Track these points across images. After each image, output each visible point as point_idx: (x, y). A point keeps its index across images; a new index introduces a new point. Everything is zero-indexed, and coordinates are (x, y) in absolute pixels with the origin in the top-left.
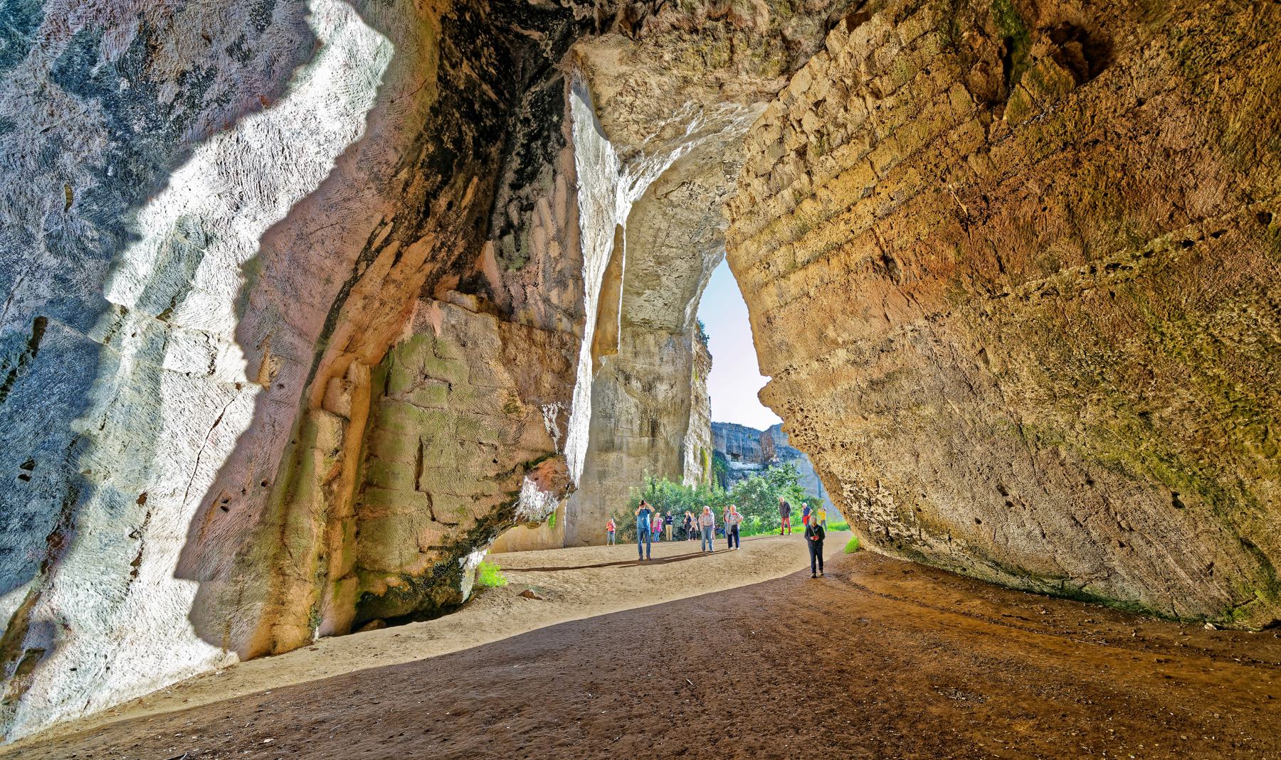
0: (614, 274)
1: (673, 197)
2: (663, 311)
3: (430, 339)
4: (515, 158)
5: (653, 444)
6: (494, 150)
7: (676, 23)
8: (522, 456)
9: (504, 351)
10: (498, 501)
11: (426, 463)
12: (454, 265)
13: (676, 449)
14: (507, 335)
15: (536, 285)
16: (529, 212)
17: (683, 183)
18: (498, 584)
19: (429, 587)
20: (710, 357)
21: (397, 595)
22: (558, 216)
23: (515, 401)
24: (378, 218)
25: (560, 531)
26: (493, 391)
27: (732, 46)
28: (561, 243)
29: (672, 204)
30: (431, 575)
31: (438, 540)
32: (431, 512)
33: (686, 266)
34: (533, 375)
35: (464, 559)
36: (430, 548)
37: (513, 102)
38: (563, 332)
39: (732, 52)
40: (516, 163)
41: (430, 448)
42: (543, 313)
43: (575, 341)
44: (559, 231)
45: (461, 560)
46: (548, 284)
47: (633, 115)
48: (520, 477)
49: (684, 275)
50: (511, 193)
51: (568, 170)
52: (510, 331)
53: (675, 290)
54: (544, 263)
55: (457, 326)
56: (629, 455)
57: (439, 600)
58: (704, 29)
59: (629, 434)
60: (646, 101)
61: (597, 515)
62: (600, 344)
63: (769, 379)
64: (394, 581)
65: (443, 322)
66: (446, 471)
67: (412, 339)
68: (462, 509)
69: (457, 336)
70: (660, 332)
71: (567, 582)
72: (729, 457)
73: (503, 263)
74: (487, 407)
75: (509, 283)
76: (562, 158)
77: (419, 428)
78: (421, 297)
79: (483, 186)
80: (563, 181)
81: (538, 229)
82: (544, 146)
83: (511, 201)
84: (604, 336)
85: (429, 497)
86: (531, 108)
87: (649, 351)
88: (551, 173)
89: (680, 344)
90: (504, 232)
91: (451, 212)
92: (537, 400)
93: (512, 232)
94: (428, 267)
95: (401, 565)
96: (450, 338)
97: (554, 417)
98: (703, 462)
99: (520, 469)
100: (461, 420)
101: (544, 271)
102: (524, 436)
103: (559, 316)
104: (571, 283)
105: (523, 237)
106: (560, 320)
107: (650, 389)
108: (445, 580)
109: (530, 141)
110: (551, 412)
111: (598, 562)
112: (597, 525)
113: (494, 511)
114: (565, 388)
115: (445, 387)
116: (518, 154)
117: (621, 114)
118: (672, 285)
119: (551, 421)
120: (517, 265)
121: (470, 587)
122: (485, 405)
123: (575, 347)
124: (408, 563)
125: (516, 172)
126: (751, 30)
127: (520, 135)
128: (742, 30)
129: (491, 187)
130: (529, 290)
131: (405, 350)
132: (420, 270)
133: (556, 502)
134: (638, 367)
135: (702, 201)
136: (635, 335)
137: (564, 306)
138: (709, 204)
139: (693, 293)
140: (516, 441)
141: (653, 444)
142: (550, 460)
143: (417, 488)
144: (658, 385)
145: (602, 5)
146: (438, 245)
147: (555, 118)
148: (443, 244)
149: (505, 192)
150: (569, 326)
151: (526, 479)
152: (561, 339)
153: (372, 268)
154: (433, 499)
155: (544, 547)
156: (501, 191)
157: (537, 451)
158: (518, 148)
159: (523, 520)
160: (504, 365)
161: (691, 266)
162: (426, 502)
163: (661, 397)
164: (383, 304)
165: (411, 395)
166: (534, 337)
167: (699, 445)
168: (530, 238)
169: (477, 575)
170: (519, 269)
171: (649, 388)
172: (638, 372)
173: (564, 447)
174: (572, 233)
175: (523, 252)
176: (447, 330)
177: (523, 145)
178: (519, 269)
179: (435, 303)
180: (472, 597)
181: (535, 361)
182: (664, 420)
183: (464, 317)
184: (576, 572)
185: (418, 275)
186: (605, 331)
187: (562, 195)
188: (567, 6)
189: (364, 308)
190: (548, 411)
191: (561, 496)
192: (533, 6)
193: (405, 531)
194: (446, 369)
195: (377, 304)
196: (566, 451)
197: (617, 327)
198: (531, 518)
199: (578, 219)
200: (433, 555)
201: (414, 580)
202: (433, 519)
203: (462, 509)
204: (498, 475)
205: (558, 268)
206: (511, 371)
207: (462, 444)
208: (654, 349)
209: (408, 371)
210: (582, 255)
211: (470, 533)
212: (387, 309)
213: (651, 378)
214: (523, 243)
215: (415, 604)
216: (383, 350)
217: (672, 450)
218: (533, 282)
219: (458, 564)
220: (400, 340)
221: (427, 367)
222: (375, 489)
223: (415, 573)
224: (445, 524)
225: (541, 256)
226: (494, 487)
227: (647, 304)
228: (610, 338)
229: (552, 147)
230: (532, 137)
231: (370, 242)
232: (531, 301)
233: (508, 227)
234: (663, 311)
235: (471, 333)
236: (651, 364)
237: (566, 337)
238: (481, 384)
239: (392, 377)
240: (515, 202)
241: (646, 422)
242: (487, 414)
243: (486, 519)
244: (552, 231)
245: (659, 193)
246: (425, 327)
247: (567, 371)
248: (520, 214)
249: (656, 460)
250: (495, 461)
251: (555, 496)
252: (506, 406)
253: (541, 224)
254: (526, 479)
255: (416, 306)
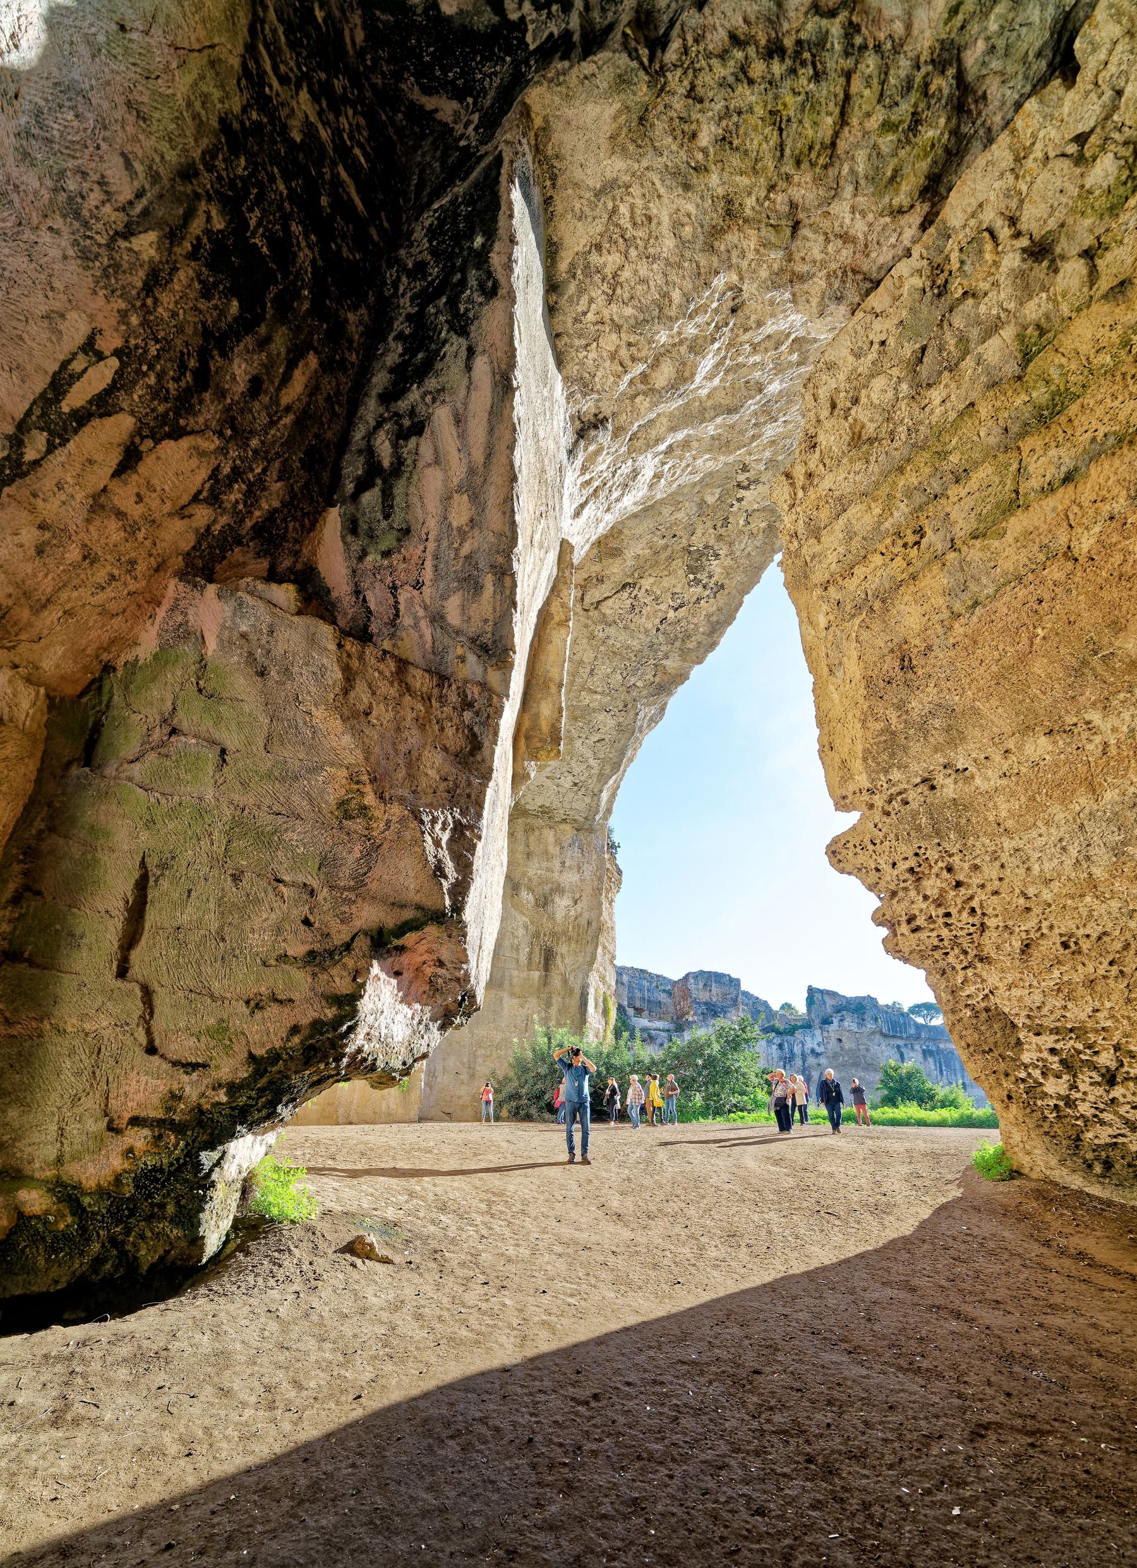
0: (557, 619)
1: (607, 608)
2: (571, 795)
3: (193, 657)
4: (392, 345)
5: (545, 981)
6: (355, 320)
7: (742, 29)
8: (368, 915)
9: (346, 692)
10: (306, 1015)
11: (152, 917)
12: (258, 530)
13: (577, 991)
14: (355, 664)
15: (418, 585)
16: (413, 441)
17: (624, 586)
18: (294, 1214)
19: (118, 1222)
20: (620, 872)
21: (37, 1238)
22: (471, 440)
23: (363, 794)
24: (76, 330)
25: (414, 1096)
26: (316, 769)
27: (847, 97)
28: (476, 499)
29: (605, 622)
30: (128, 1190)
31: (155, 1100)
32: (149, 1032)
33: (611, 723)
34: (403, 748)
35: (215, 1155)
36: (135, 1121)
37: (399, 237)
38: (466, 682)
39: (843, 119)
40: (394, 353)
41: (165, 884)
42: (429, 645)
43: (490, 699)
44: (472, 471)
45: (207, 1158)
46: (442, 585)
47: (614, 307)
48: (362, 963)
49: (607, 737)
50: (381, 410)
51: (499, 344)
52: (361, 658)
53: (592, 762)
54: (438, 540)
55: (252, 637)
56: (512, 994)
57: (147, 1255)
58: (799, 42)
59: (513, 965)
60: (643, 271)
61: (464, 1077)
62: (527, 738)
63: (854, 817)
64: (34, 1200)
65: (223, 627)
66: (195, 937)
67: (156, 657)
68: (220, 1031)
69: (250, 654)
70: (563, 826)
71: (443, 1208)
72: (630, 1011)
73: (356, 546)
74: (300, 803)
75: (364, 585)
76: (490, 317)
77: (144, 836)
78: (182, 575)
79: (327, 385)
80: (487, 368)
81: (429, 471)
82: (453, 303)
83: (379, 425)
84: (535, 725)
85: (147, 994)
86: (430, 242)
87: (546, 852)
88: (464, 354)
89: (589, 844)
90: (363, 485)
91: (257, 406)
92: (410, 797)
93: (379, 482)
94: (203, 515)
95: (59, 1161)
96: (235, 659)
97: (445, 837)
98: (605, 1012)
99: (362, 944)
100: (239, 826)
101: (436, 557)
102: (378, 871)
103: (460, 651)
104: (488, 581)
105: (399, 489)
106: (463, 659)
107: (545, 904)
108: (162, 1206)
109: (423, 307)
110: (438, 826)
111: (494, 1161)
112: (463, 1091)
113: (296, 1040)
114: (469, 784)
115: (212, 755)
116: (400, 337)
117: (591, 301)
118: (589, 754)
119: (437, 843)
120: (383, 547)
121: (226, 1224)
122: (296, 799)
123: (491, 710)
124: (76, 1157)
125: (391, 371)
126: (896, 50)
127: (405, 302)
128: (878, 48)
129: (344, 399)
130: (404, 596)
131: (139, 677)
132: (182, 512)
133: (436, 1034)
134: (531, 873)
135: (648, 618)
136: (528, 830)
137: (472, 630)
138: (658, 621)
139: (616, 766)
140: (359, 882)
141: (545, 981)
142: (431, 930)
143: (122, 972)
144: (557, 899)
145: (587, 7)
146: (226, 470)
147: (479, 241)
148: (237, 474)
149: (371, 409)
150: (479, 671)
151: (376, 969)
152: (462, 694)
153: (60, 456)
154: (157, 1001)
155: (391, 1119)
156: (362, 410)
157: (403, 906)
158: (401, 325)
159: (362, 1066)
160: (345, 720)
161: (619, 725)
162: (136, 1007)
163: (559, 916)
164: (89, 557)
165: (137, 766)
166: (409, 679)
167: (602, 989)
168: (412, 489)
169: (245, 1191)
170: (386, 554)
171: (544, 902)
172: (530, 880)
173: (463, 903)
174: (496, 477)
175: (397, 520)
176: (231, 642)
177: (409, 318)
178: (386, 554)
179: (212, 589)
180: (232, 1246)
181: (408, 722)
182: (562, 949)
183: (268, 619)
184: (459, 1182)
185: (178, 525)
186: (537, 716)
187: (483, 396)
188: (514, 16)
189: (40, 551)
190: (434, 821)
191: (446, 1020)
192: (449, 19)
193: (79, 1074)
194: (219, 720)
195: (73, 554)
196: (468, 915)
197: (560, 710)
198: (380, 1064)
199: (511, 448)
200: (139, 1139)
201: (86, 1200)
202: (151, 1050)
203: (220, 1031)
204: (311, 954)
205: (466, 550)
206: (357, 733)
207: (236, 878)
208: (554, 850)
209: (135, 718)
210: (513, 524)
211: (233, 1088)
212: (101, 576)
213: (547, 888)
214: (399, 500)
215: (81, 1264)
216: (86, 669)
217: (572, 991)
218: (412, 580)
219: (198, 1165)
220: (130, 657)
221: (180, 713)
222: (23, 967)
223: (90, 1184)
224: (175, 1064)
225: (432, 524)
226: (300, 981)
227: (549, 783)
228: (545, 727)
229: (470, 300)
230: (425, 298)
231: (60, 383)
232: (406, 620)
233: (374, 474)
234: (571, 795)
235: (279, 650)
236: (548, 870)
237: (473, 692)
238: (292, 755)
239: (105, 732)
240: (387, 427)
241: (537, 949)
242: (298, 817)
243: (274, 1057)
244: (458, 471)
245: (588, 599)
246: (185, 633)
247: (472, 753)
248: (395, 446)
249: (548, 1004)
250: (307, 922)
251: (433, 1019)
252: (342, 804)
253: (437, 461)
254: (376, 969)
255: (171, 592)
